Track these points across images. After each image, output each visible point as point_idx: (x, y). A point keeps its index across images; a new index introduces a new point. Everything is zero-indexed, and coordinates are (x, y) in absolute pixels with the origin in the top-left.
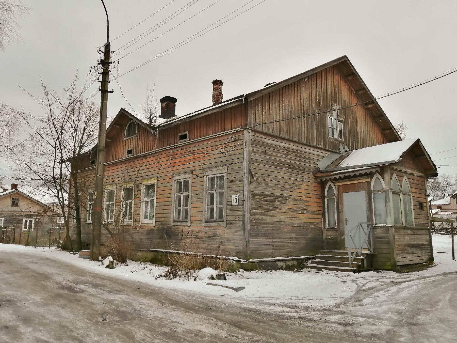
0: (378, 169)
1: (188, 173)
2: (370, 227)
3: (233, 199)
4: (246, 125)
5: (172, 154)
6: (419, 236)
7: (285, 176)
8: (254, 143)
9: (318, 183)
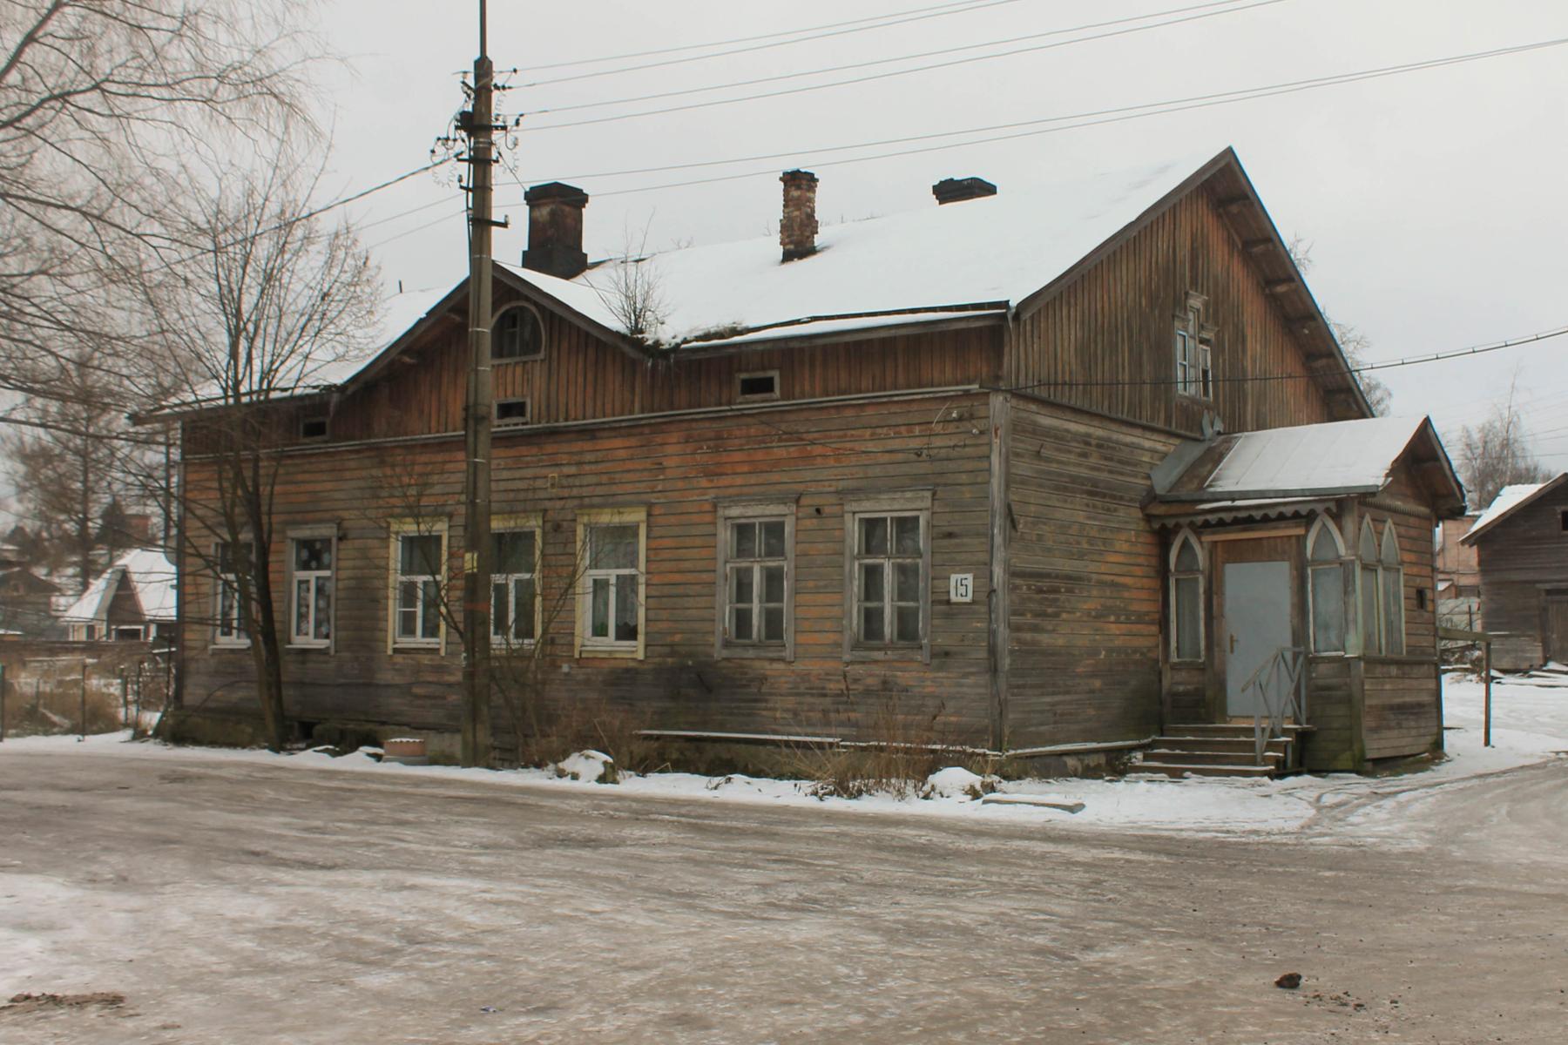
0: (1332, 506)
1: (782, 500)
2: (1301, 659)
3: (953, 583)
4: (998, 378)
5: (712, 435)
6: (1415, 683)
7: (1080, 517)
8: (1018, 428)
9: (1154, 532)
